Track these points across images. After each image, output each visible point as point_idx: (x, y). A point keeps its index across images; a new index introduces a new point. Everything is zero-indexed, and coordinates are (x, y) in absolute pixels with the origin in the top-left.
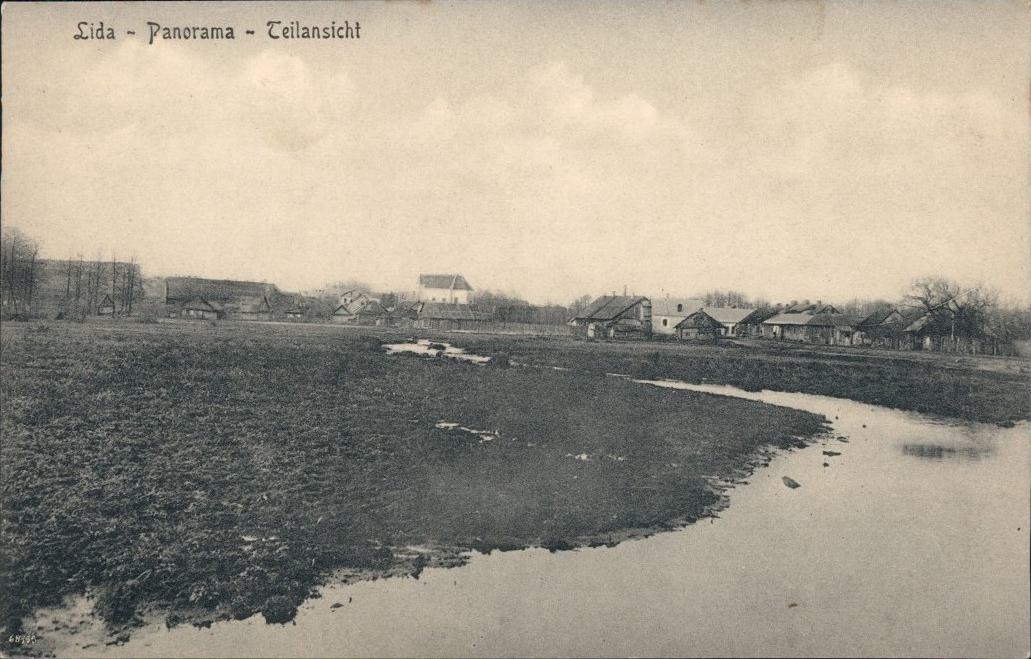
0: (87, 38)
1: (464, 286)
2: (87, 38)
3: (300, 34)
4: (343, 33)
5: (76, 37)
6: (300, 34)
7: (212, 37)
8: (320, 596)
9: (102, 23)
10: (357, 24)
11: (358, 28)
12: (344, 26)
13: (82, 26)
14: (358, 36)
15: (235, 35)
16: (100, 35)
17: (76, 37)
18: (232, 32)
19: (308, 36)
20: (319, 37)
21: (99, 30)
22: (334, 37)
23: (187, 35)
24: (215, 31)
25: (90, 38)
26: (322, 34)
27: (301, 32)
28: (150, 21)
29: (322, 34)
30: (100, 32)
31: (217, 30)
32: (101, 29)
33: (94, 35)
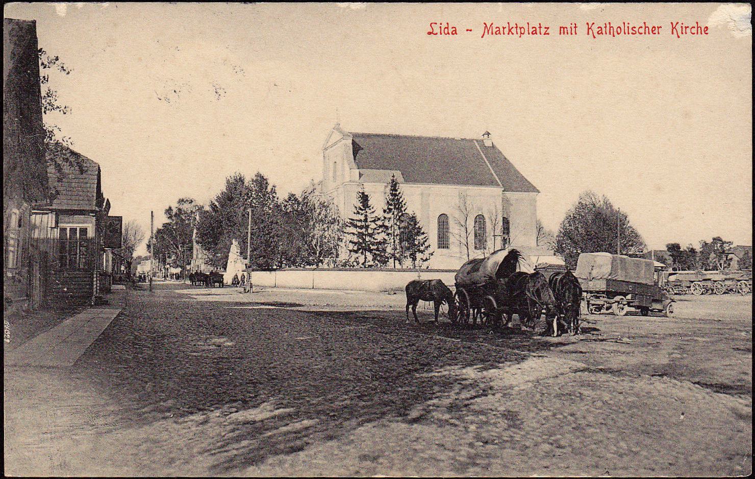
0: (436, 34)
1: (531, 189)
2: (436, 34)
3: (530, 32)
4: (642, 30)
5: (429, 33)
6: (530, 32)
7: (564, 33)
8: (236, 275)
9: (448, 24)
10: (540, 24)
11: (575, 27)
12: (696, 26)
13: (634, 29)
14: (576, 34)
15: (457, 32)
16: (446, 32)
17: (429, 33)
18: (455, 31)
19: (536, 33)
20: (629, 33)
21: (445, 28)
22: (441, 34)
23: (619, 32)
24: (562, 29)
25: (643, 34)
26: (631, 31)
27: (531, 30)
28: (530, 24)
29: (631, 31)
30: (446, 30)
31: (564, 28)
32: (448, 28)
33: (442, 32)
